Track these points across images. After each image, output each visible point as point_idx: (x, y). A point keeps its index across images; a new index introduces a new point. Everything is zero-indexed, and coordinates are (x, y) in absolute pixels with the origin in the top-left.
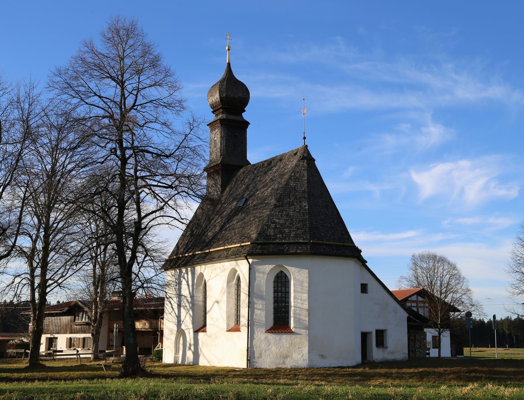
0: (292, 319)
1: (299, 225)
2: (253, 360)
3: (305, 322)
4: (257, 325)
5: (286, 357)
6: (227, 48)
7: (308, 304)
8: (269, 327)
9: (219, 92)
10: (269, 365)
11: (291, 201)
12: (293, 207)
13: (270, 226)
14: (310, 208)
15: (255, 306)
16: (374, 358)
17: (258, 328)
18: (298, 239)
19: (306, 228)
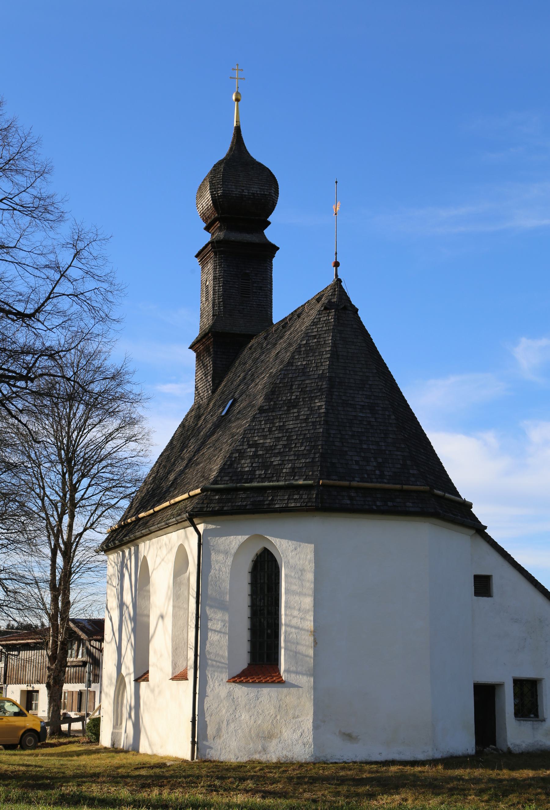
0: (283, 652)
1: (303, 448)
2: (205, 742)
3: (308, 659)
4: (213, 666)
5: (270, 736)
6: (234, 98)
7: (312, 618)
8: (238, 670)
9: (210, 186)
10: (235, 755)
11: (293, 397)
12: (295, 410)
13: (244, 452)
14: (331, 411)
15: (210, 624)
16: (509, 744)
17: (214, 671)
18: (296, 478)
19: (315, 453)
